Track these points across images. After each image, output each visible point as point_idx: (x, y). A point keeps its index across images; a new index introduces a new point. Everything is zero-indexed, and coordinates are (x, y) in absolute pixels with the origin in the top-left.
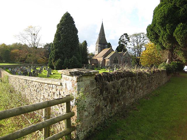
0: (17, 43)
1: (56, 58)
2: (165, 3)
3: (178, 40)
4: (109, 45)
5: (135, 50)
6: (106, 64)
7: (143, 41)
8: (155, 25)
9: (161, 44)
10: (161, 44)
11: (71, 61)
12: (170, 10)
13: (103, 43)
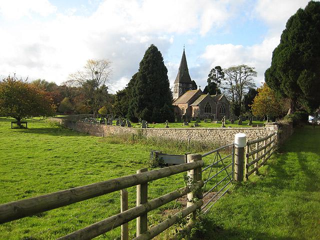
0: (40, 81)
1: (141, 106)
2: (287, 46)
3: (303, 88)
4: (194, 86)
5: (232, 92)
6: (193, 114)
7: (245, 78)
8: (275, 70)
9: (282, 92)
10: (282, 92)
11: (162, 112)
12: (293, 55)
13: (186, 82)
